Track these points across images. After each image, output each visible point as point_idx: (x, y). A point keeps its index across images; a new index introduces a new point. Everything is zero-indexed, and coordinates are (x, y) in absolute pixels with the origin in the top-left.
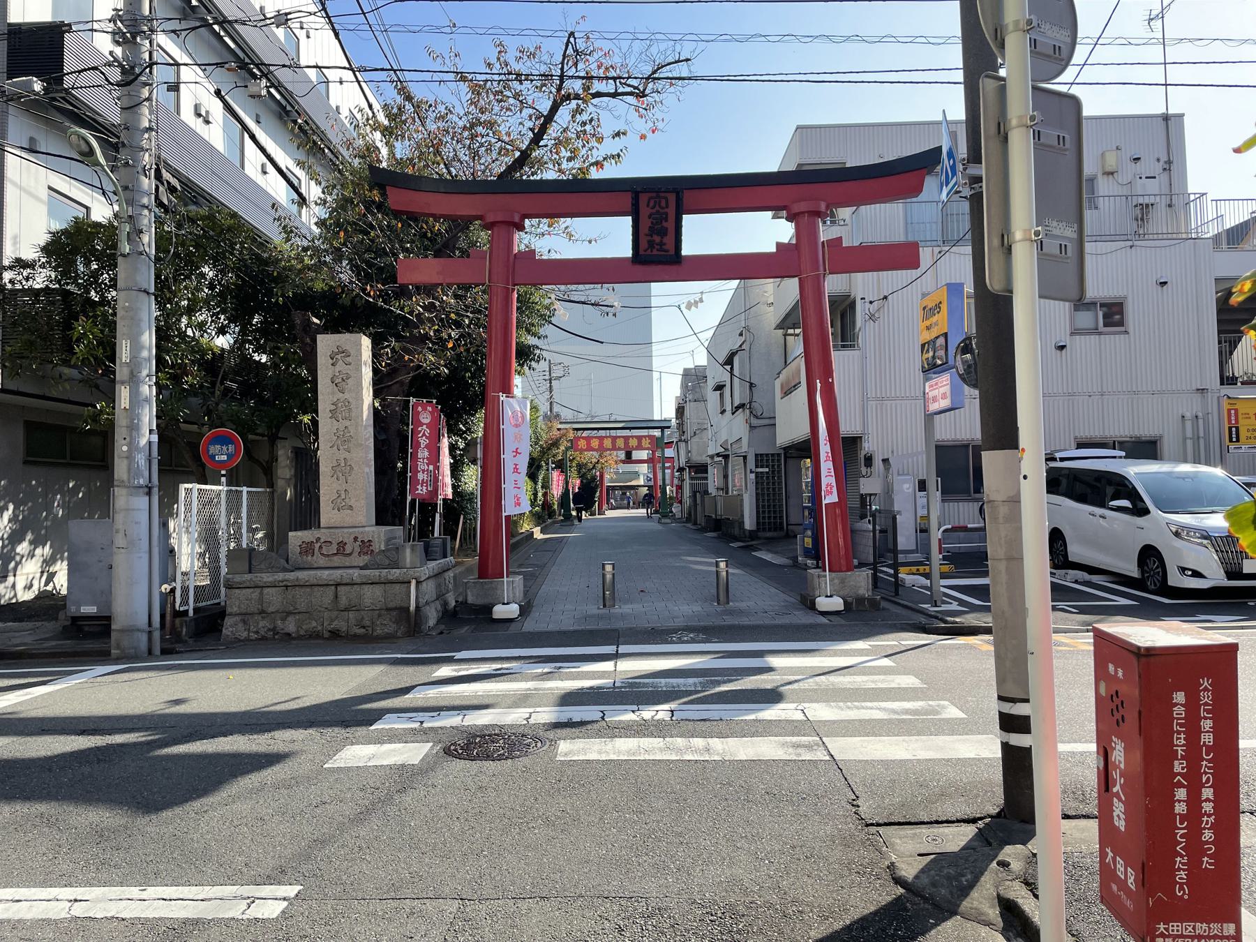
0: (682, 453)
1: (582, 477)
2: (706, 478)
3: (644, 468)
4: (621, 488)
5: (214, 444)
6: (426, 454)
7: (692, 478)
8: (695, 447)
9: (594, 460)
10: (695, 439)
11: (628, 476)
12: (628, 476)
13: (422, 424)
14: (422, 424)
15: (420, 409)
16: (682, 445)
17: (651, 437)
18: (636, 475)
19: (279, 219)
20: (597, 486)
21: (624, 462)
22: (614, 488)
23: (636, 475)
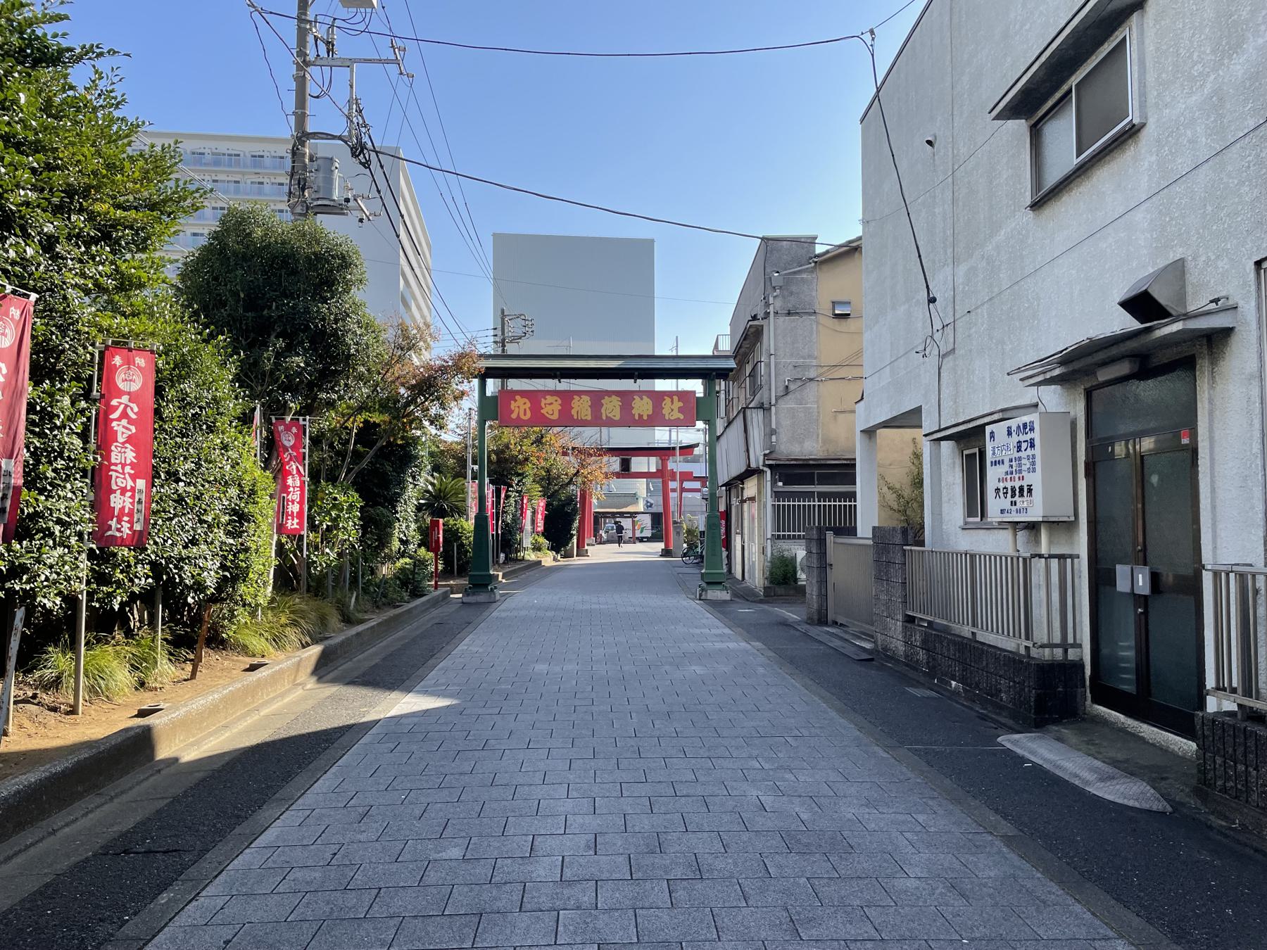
0: (756, 434)
1: (549, 495)
2: (852, 496)
3: (640, 486)
4: (613, 515)
5: (356, 491)
6: (130, 455)
7: (777, 495)
8: (786, 422)
9: (572, 471)
10: (787, 404)
11: (622, 500)
12: (622, 500)
13: (120, 393)
14: (120, 393)
15: (117, 360)
16: (756, 418)
17: (684, 396)
18: (634, 497)
19: (105, 234)
20: (575, 511)
21: (618, 475)
22: (605, 515)
23: (634, 497)
